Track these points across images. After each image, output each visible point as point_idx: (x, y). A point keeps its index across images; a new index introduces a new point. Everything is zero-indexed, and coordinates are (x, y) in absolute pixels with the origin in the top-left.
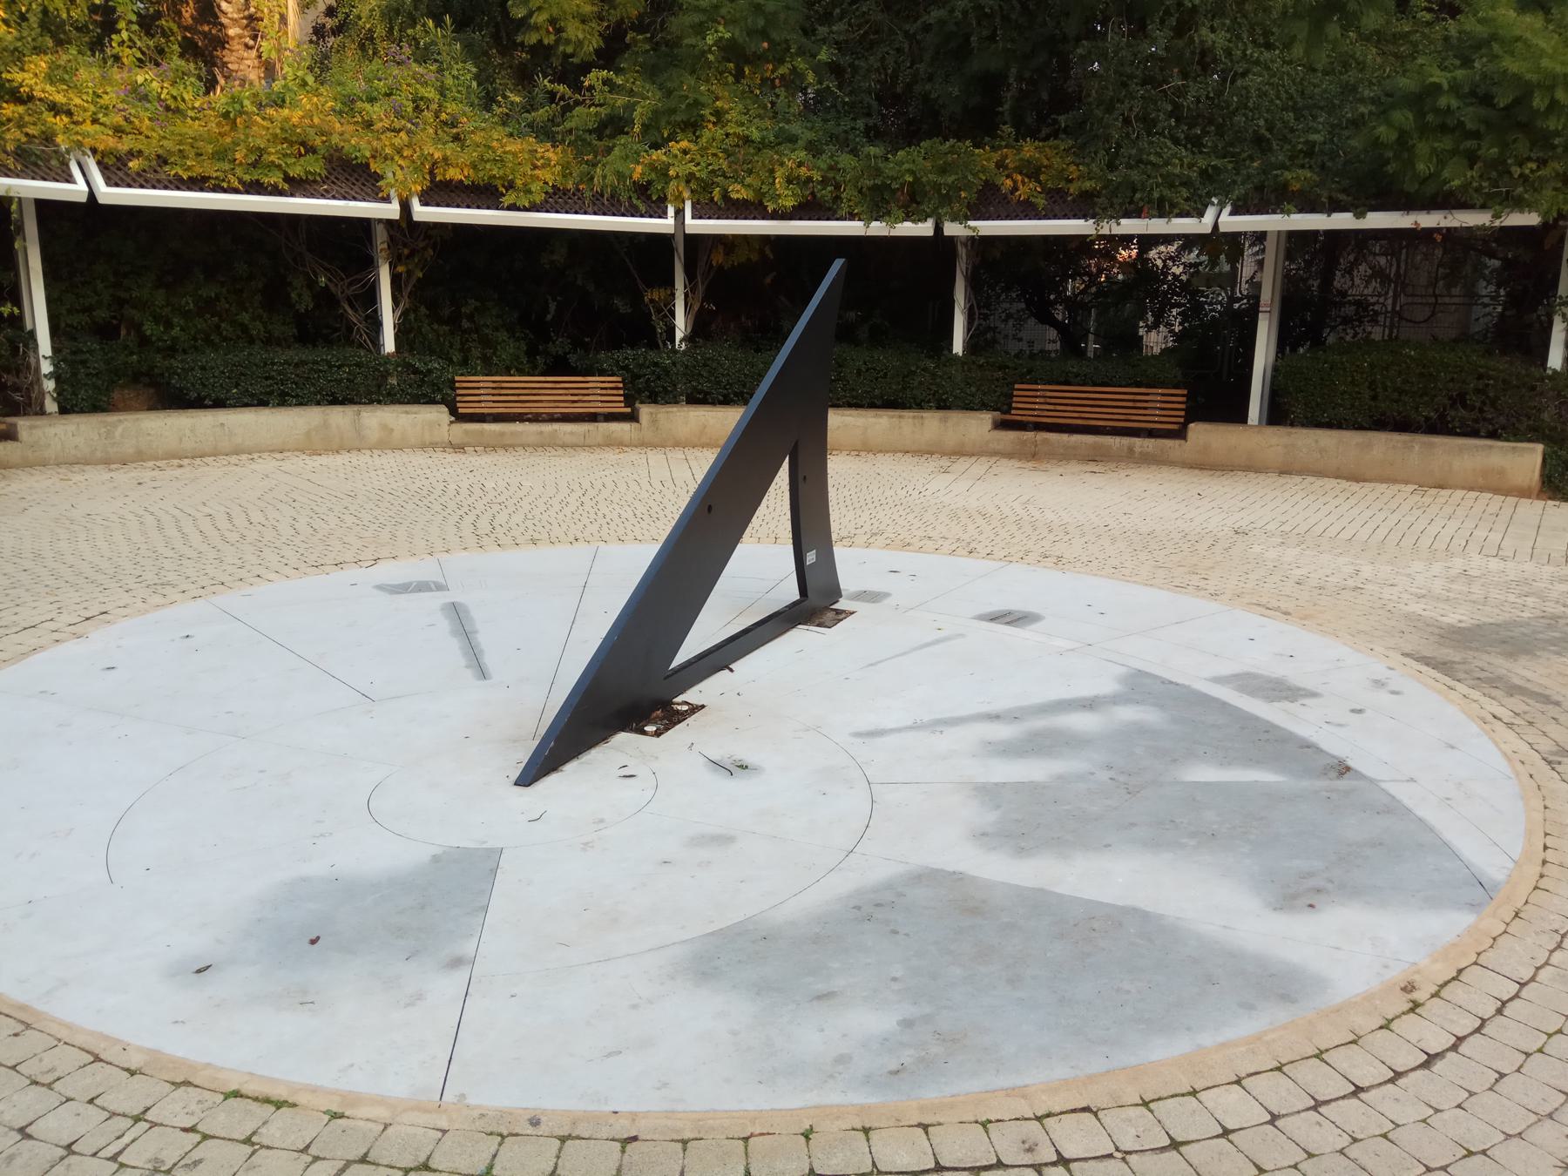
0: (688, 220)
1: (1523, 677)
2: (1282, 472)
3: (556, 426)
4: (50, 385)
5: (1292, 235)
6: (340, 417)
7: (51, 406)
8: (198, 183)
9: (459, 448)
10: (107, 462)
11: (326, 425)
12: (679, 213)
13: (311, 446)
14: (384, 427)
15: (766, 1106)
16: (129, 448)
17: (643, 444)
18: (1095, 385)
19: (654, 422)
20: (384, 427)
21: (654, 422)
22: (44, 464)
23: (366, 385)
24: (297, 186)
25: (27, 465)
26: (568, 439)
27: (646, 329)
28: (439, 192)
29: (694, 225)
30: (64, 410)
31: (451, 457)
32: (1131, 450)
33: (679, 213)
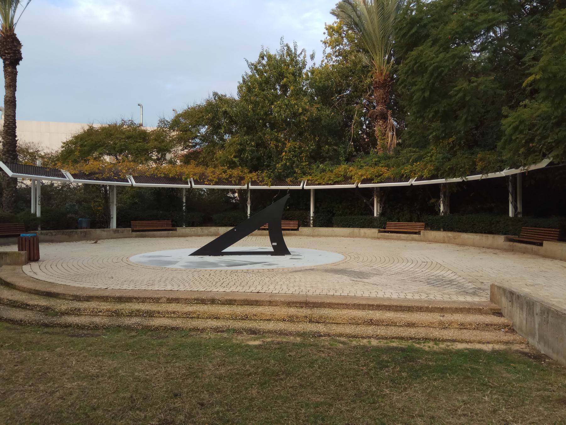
0: (250, 186)
2: (561, 260)
3: (393, 234)
4: (312, 222)
6: (356, 230)
7: (312, 226)
8: (319, 184)
9: (378, 238)
10: (313, 236)
14: (365, 233)
16: (316, 234)
17: (421, 241)
18: (544, 227)
19: (424, 235)
20: (365, 233)
21: (424, 235)
23: (368, 223)
24: (335, 183)
26: (403, 238)
27: (434, 211)
28: (363, 182)
29: (251, 187)
30: (313, 226)
31: (377, 240)
32: (362, 234)
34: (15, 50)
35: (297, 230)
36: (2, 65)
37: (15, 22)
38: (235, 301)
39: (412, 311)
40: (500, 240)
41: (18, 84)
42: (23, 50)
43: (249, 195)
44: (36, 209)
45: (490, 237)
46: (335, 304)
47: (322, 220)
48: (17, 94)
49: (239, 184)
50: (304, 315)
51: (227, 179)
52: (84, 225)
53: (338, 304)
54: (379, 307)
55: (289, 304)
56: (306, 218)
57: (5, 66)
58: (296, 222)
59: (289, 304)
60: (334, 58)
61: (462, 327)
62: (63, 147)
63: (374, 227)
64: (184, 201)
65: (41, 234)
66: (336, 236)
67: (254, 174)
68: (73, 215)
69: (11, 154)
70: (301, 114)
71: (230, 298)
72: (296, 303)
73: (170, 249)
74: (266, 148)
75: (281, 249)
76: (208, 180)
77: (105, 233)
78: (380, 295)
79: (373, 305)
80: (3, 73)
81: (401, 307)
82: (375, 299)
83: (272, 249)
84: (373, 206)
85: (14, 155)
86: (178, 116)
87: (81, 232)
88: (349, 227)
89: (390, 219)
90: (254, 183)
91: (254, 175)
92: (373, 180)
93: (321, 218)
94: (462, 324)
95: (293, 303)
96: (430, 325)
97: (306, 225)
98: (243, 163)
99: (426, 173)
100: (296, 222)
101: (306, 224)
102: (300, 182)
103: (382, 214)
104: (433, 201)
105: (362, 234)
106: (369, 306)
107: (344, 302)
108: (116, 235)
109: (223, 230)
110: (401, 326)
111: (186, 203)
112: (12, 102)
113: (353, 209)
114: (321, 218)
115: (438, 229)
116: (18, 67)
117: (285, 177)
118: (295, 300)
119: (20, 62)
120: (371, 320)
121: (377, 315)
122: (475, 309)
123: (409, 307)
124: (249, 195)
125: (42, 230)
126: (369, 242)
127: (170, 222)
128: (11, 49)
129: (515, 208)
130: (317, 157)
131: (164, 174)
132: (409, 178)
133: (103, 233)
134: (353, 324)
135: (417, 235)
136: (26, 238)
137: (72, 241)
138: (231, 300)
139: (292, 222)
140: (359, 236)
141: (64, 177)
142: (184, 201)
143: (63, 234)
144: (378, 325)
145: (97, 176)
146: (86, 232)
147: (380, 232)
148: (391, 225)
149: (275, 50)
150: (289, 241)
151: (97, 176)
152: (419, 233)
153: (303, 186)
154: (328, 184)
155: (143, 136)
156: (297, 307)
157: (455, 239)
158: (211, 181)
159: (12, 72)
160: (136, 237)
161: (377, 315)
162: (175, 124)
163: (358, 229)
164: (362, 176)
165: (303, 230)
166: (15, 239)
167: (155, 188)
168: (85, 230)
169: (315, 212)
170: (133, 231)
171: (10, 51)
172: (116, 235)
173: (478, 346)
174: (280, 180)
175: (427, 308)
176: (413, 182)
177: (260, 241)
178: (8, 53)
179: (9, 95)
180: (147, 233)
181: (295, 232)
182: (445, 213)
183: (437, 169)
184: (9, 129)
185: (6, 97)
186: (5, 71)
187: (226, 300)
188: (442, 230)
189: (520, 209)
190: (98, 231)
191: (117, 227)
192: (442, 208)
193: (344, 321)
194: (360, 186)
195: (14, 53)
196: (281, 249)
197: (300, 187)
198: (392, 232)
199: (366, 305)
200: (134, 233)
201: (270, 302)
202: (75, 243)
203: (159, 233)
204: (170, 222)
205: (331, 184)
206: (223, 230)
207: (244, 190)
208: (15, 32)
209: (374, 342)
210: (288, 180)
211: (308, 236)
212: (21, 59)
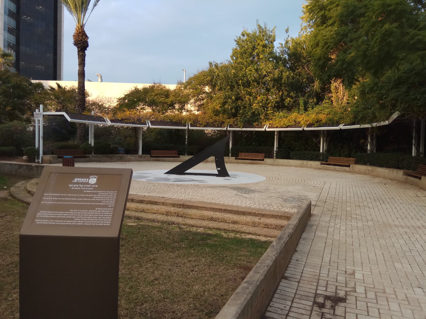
0: (228, 128)
1: (205, 227)
3: (336, 167)
4: (275, 155)
5: (279, 131)
6: (305, 162)
7: (275, 158)
9: (320, 169)
11: (303, 163)
12: (188, 126)
13: (302, 166)
14: (311, 165)
15: (261, 258)
19: (352, 167)
20: (311, 165)
21: (352, 167)
22: (266, 164)
24: (287, 127)
25: (264, 164)
26: (338, 170)
28: (308, 126)
30: (276, 158)
32: (309, 165)
33: (188, 126)
34: (84, 41)
35: (263, 160)
36: (77, 51)
37: (84, 23)
38: (144, 201)
39: (245, 215)
40: (399, 174)
41: (86, 62)
42: (89, 41)
43: (231, 134)
44: (91, 141)
45: (395, 171)
46: (200, 207)
47: (282, 154)
48: (86, 69)
49: (221, 127)
50: (175, 211)
51: (213, 123)
52: (121, 152)
53: (201, 207)
54: (220, 210)
55: (173, 205)
56: (271, 152)
57: (78, 52)
58: (263, 155)
59: (173, 205)
60: (309, 30)
61: (266, 226)
62: (118, 101)
63: (319, 160)
64: (187, 137)
65: (93, 156)
66: (290, 166)
67: (232, 119)
68: (115, 145)
69: (82, 107)
70: (265, 76)
71: (142, 199)
72: (178, 204)
73: (161, 169)
74: (243, 100)
75: (223, 173)
76: (200, 124)
77: (133, 157)
78: (239, 204)
79: (222, 209)
80: (77, 56)
81: (238, 211)
82: (223, 205)
83: (217, 173)
84: (320, 145)
85: (83, 107)
86: (190, 79)
87: (118, 156)
88: (301, 160)
89: (332, 155)
90: (231, 126)
91: (232, 120)
92: (314, 124)
93: (282, 152)
94: (266, 225)
95: (176, 204)
96: (247, 224)
97: (271, 157)
98: (224, 112)
99: (348, 120)
100: (263, 155)
101: (269, 155)
102: (264, 126)
103: (327, 151)
104: (362, 141)
105: (309, 165)
106: (220, 209)
107: (205, 206)
108: (140, 159)
109: (186, 158)
110: (229, 223)
111: (188, 139)
112: (82, 74)
113: (307, 146)
114: (282, 152)
115: (365, 164)
116: (86, 51)
117: (253, 122)
118: (177, 203)
119: (88, 48)
120: (212, 218)
121: (218, 215)
122: (285, 217)
123: (243, 212)
124: (231, 134)
125: (94, 154)
126: (316, 172)
127: (176, 152)
128: (81, 40)
129: (418, 149)
130: (280, 106)
131: (170, 119)
132: (340, 124)
133: (132, 157)
134: (201, 219)
135: (347, 168)
136: (66, 158)
137: (112, 162)
138: (142, 201)
139: (260, 155)
140: (307, 167)
141: (104, 121)
142: (187, 137)
143: (107, 157)
144: (215, 221)
145: (126, 121)
146: (121, 157)
147: (322, 164)
148: (332, 159)
149: (252, 29)
150: (228, 167)
151: (126, 121)
152: (349, 166)
153: (266, 128)
154: (282, 127)
155: (167, 93)
156: (177, 207)
157: (373, 172)
158: (201, 124)
159: (82, 55)
160: (154, 161)
161: (218, 215)
162: (189, 83)
163: (306, 161)
164: (307, 121)
165: (268, 160)
166: (61, 159)
167: (160, 129)
168: (121, 155)
169: (278, 148)
170: (151, 157)
171: (81, 42)
172: (141, 159)
173: (253, 237)
174: (249, 123)
175: (255, 213)
176: (341, 127)
177: (209, 166)
178: (80, 43)
179: (81, 70)
180: (160, 158)
181: (261, 162)
182: (372, 151)
183: (355, 117)
184: (80, 91)
185: (79, 70)
186: (78, 54)
187: (139, 200)
188: (368, 164)
189: (421, 150)
190: (129, 156)
191: (142, 154)
192: (369, 147)
193: (197, 217)
194: (306, 129)
195: (83, 43)
196: (223, 173)
197: (263, 129)
198: (333, 165)
199: (217, 209)
200: (152, 158)
201: (163, 203)
202: (113, 163)
203: (168, 159)
204: (176, 152)
205: (284, 128)
206: (186, 158)
207: (224, 131)
208: (85, 29)
209: (200, 230)
210: (255, 124)
211: (270, 165)
212: (88, 46)
